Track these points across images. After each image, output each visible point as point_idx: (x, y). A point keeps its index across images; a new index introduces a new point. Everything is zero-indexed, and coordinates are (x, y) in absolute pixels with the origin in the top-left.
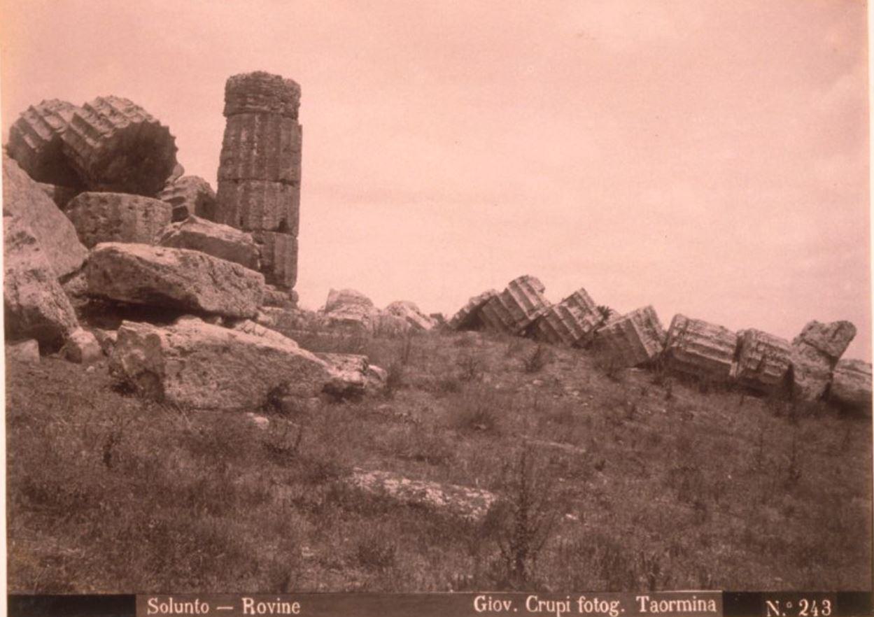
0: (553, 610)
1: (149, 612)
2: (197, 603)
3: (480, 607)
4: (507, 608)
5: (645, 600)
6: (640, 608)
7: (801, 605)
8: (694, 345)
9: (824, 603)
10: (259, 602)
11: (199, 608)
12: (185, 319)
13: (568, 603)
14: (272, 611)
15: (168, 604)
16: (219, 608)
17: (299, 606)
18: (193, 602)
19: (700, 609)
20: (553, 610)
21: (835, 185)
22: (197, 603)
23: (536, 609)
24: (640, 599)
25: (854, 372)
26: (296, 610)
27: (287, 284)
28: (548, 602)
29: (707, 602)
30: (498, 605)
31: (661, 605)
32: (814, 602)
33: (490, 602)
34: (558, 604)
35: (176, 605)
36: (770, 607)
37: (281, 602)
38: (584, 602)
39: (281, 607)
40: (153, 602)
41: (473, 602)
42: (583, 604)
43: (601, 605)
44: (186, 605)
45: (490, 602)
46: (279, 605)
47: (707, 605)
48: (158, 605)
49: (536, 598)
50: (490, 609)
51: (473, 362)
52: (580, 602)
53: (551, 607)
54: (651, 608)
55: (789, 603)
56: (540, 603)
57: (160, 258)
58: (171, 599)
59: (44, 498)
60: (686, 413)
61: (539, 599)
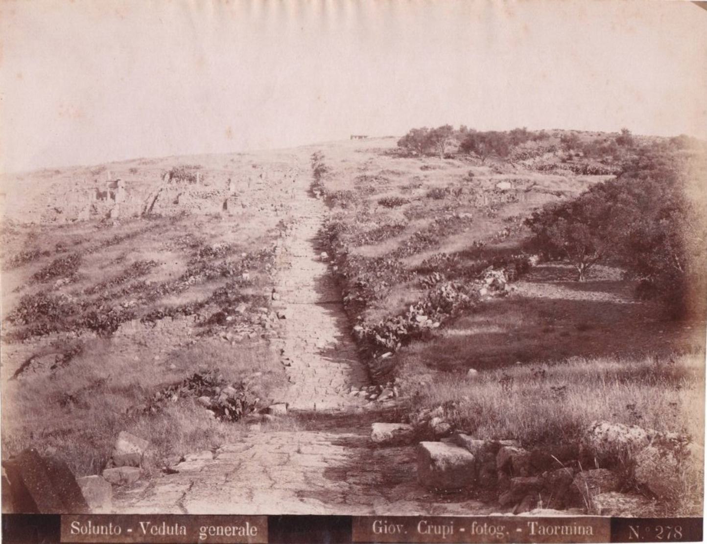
0: (440, 532)
1: (72, 532)
2: (485, 526)
3: (378, 530)
5: (535, 525)
7: (657, 530)
8: (480, 324)
11: (113, 531)
13: (452, 527)
17: (256, 530)
18: (573, 526)
20: (440, 532)
21: (272, 205)
22: (111, 526)
36: (632, 532)
38: (476, 526)
40: (76, 525)
41: (372, 524)
43: (394, 530)
47: (586, 530)
48: (80, 527)
52: (473, 526)
57: (79, 246)
58: (248, 524)
60: (21, 380)
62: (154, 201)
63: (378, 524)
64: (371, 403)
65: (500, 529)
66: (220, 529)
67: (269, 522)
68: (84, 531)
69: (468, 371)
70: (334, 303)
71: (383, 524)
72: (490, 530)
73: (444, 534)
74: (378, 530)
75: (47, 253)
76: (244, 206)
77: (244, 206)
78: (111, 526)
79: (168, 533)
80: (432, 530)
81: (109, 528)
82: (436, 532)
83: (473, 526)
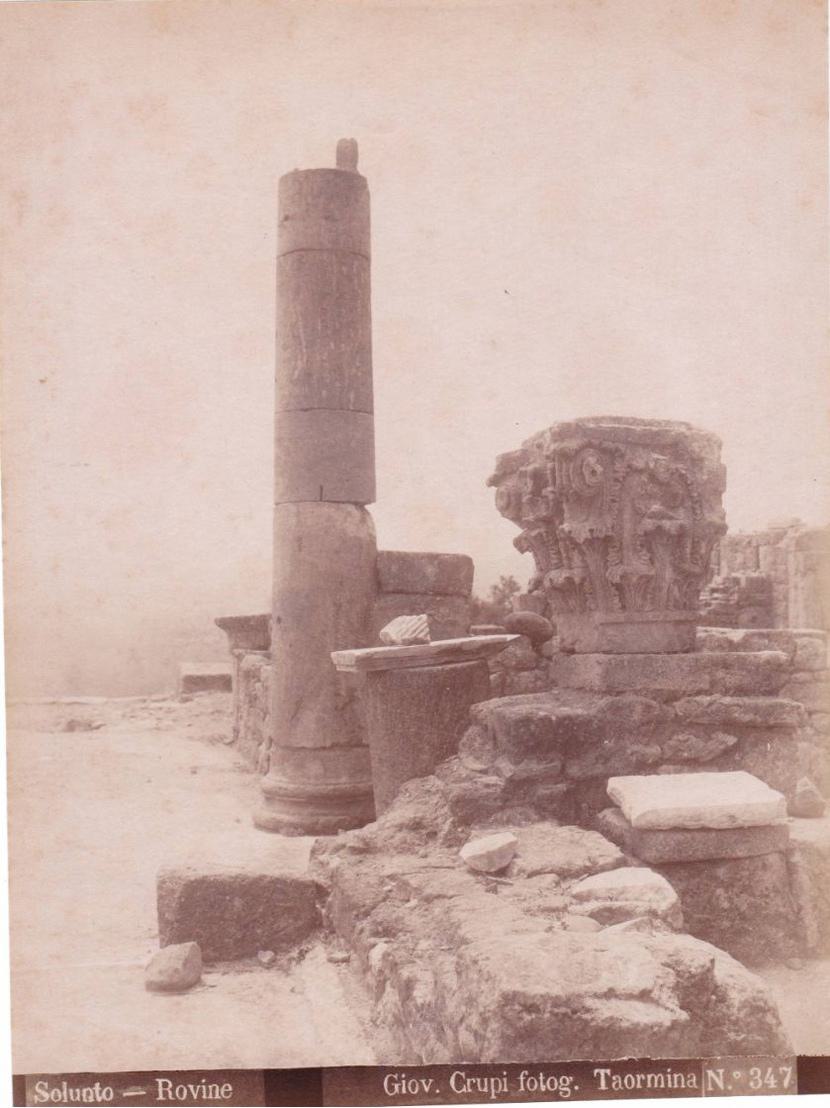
4: (427, 1089)
5: (606, 1074)
9: (781, 1072)
10: (178, 1085)
12: (278, 371)
13: (505, 1080)
14: (195, 1096)
15: (62, 1091)
16: (125, 1094)
17: (230, 1089)
18: (665, 1073)
19: (656, 1085)
20: (486, 1090)
22: (541, 1078)
23: (464, 1090)
24: (598, 1074)
26: (227, 1093)
28: (479, 1080)
29: (685, 1076)
30: (181, 1091)
31: (626, 1081)
32: (770, 1070)
33: (404, 1082)
34: (492, 1080)
35: (71, 1091)
37: (206, 1084)
38: (526, 1077)
39: (208, 1090)
41: (384, 1078)
42: (525, 1081)
43: (626, 1081)
44: (85, 1091)
45: (404, 1082)
46: (204, 1087)
48: (49, 1091)
49: (463, 1074)
50: (404, 1091)
52: (522, 1078)
53: (483, 1086)
54: (614, 1085)
55: (734, 1074)
56: (469, 1081)
58: (65, 1084)
59: (210, 941)
61: (468, 1076)
63: (391, 1080)
64: (388, 871)
65: (564, 1081)
66: (214, 1088)
67: (265, 1077)
68: (552, 1086)
70: (818, 670)
71: (400, 1080)
72: (528, 1085)
73: (493, 1091)
74: (391, 1088)
75: (393, 643)
76: (324, 632)
77: (324, 632)
78: (541, 1078)
79: (72, 1098)
80: (474, 1086)
81: (539, 1081)
82: (480, 1089)
83: (522, 1078)
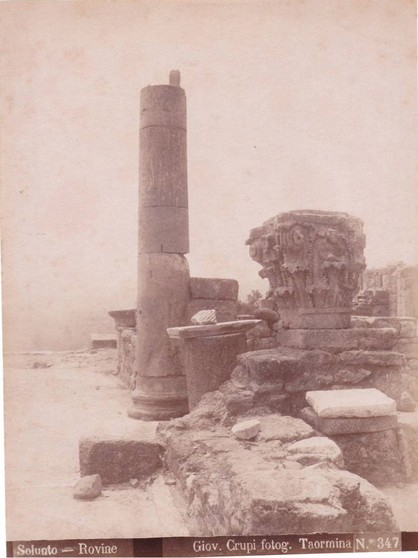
4: (215, 548)
5: (305, 541)
6: (79, 552)
9: (393, 540)
10: (89, 546)
13: (254, 544)
14: (98, 552)
15: (31, 549)
16: (63, 551)
17: (116, 548)
18: (335, 540)
19: (330, 547)
20: (245, 549)
22: (273, 543)
23: (234, 549)
24: (301, 541)
25: (148, 402)
26: (114, 551)
27: (235, 298)
28: (241, 544)
29: (345, 542)
30: (91, 549)
31: (315, 545)
32: (388, 539)
33: (203, 545)
34: (248, 544)
35: (36, 549)
37: (104, 546)
38: (265, 542)
39: (105, 549)
41: (193, 543)
42: (264, 544)
43: (315, 545)
44: (43, 549)
45: (203, 545)
46: (103, 547)
48: (24, 550)
49: (233, 541)
50: (203, 550)
51: (252, 347)
52: (263, 543)
53: (243, 547)
54: (309, 546)
55: (370, 541)
56: (236, 544)
58: (33, 546)
61: (235, 542)
62: (304, 438)
63: (197, 544)
64: (195, 439)
65: (284, 544)
66: (108, 548)
67: (133, 542)
69: (384, 364)
71: (201, 544)
72: (266, 546)
73: (248, 549)
74: (197, 548)
76: (163, 319)
77: (163, 319)
78: (273, 543)
79: (36, 553)
80: (239, 547)
81: (271, 544)
82: (242, 549)
83: (263, 543)
